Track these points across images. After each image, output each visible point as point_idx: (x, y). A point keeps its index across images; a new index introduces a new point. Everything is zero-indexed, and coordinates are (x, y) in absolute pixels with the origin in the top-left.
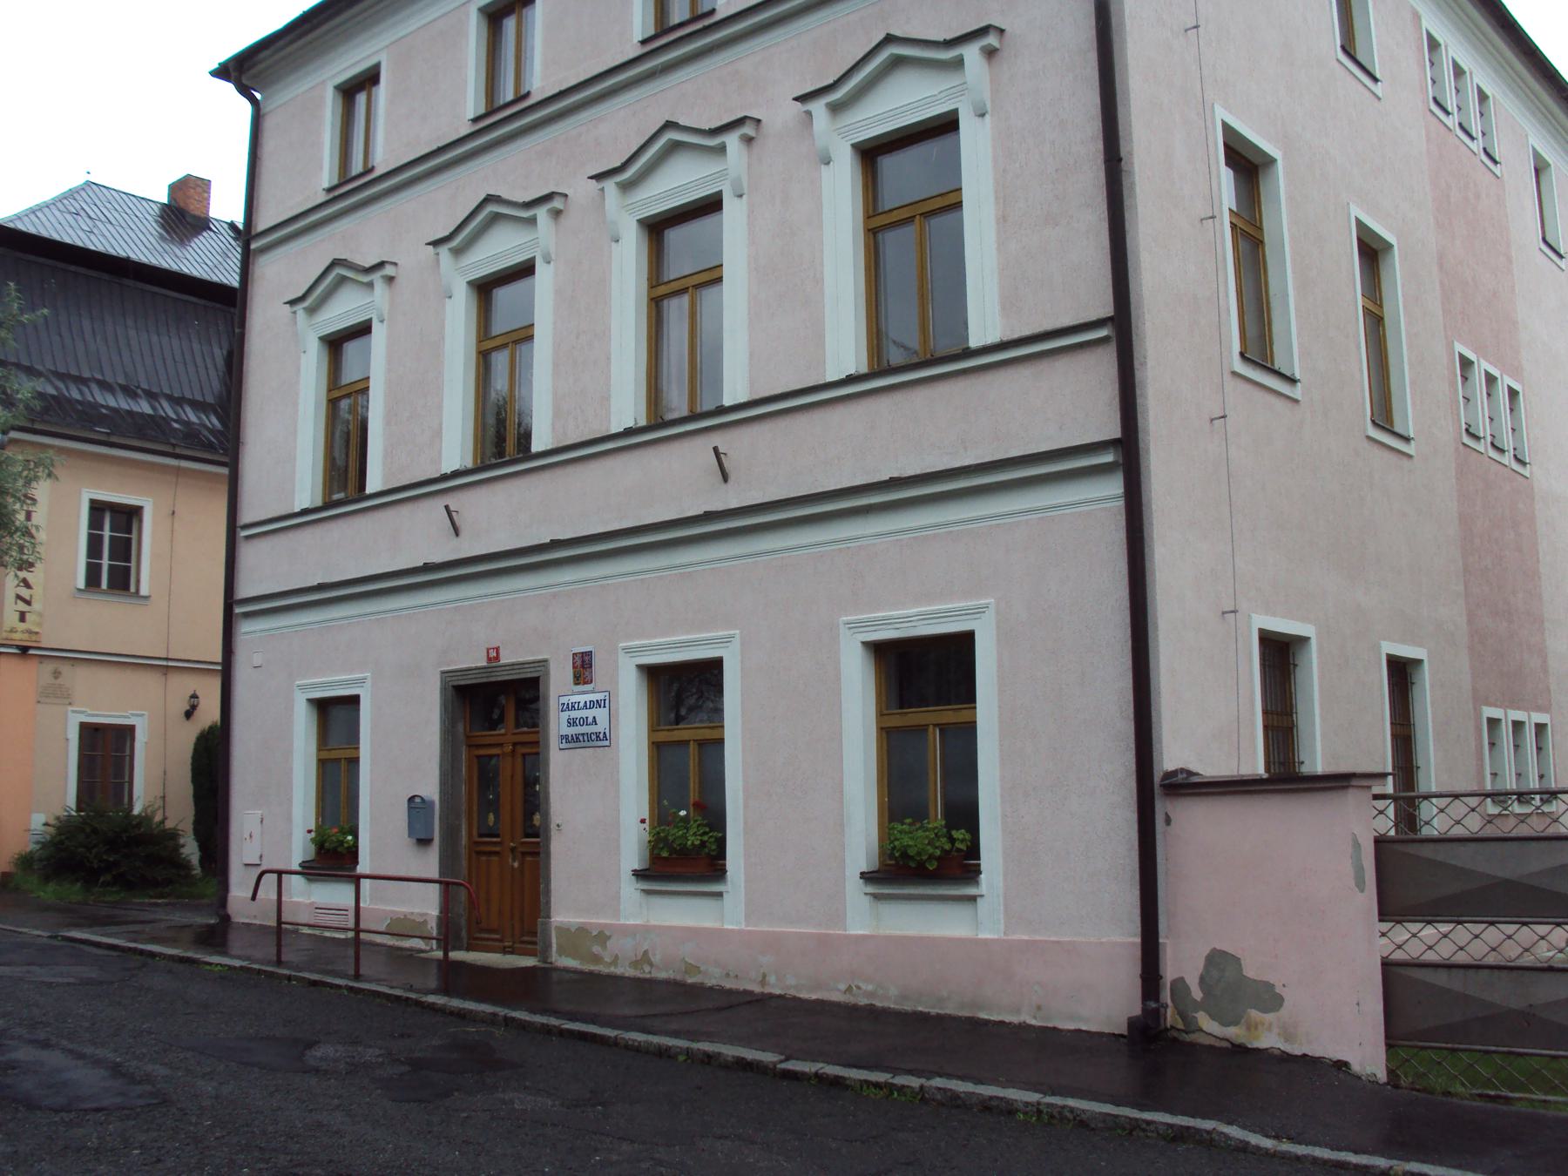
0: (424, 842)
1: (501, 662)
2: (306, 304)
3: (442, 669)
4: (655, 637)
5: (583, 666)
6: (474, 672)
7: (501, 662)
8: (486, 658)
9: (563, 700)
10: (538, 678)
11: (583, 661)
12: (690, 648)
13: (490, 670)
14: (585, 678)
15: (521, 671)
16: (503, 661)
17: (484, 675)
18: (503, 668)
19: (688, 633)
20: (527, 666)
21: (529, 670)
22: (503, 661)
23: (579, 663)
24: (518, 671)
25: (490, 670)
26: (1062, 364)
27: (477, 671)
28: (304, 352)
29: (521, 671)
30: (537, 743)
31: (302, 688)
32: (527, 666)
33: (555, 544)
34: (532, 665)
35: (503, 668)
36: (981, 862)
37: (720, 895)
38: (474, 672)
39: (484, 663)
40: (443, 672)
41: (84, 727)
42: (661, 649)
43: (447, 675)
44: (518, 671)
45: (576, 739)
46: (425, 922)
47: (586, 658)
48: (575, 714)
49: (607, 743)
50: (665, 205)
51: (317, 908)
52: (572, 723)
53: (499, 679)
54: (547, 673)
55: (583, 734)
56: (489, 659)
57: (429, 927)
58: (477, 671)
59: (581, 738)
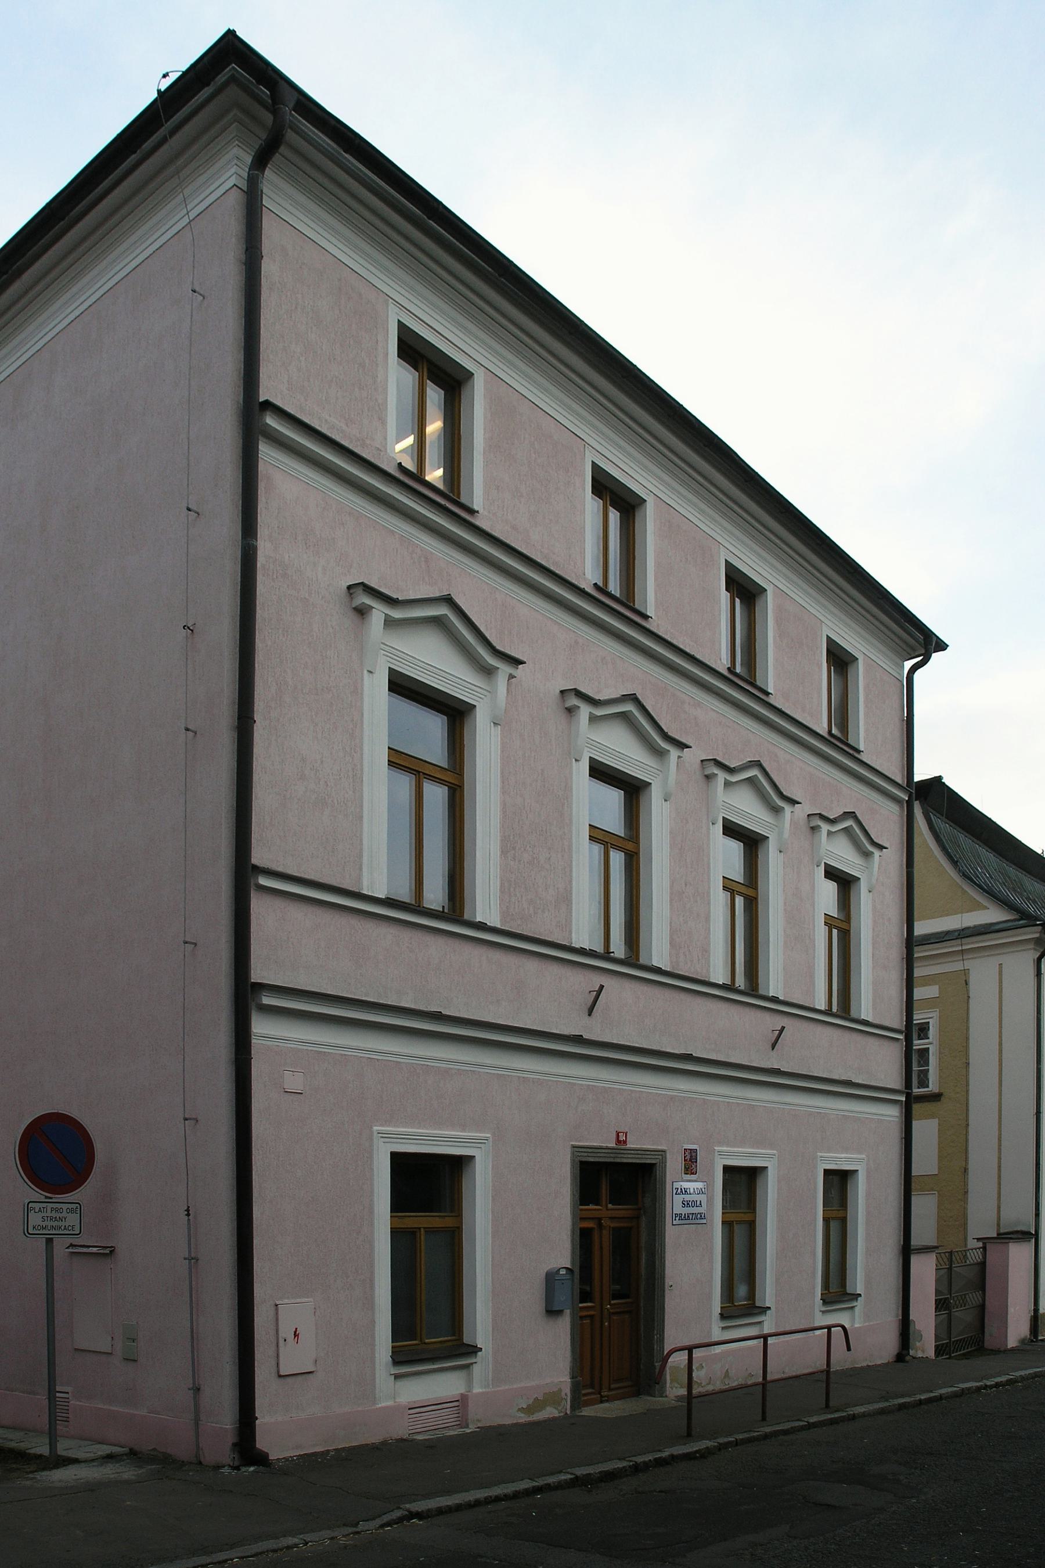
0: (552, 1312)
1: (628, 1146)
2: (397, 614)
3: (573, 1143)
4: (734, 1147)
5: (690, 1160)
6: (604, 1151)
7: (628, 1146)
8: (614, 1140)
9: (676, 1185)
10: (654, 1164)
11: (691, 1156)
12: (754, 1158)
13: (618, 1151)
14: (692, 1170)
15: (644, 1156)
16: (629, 1146)
17: (612, 1155)
18: (629, 1152)
19: (753, 1147)
20: (648, 1153)
21: (649, 1157)
22: (629, 1146)
23: (688, 1157)
24: (640, 1156)
25: (618, 1151)
26: (886, 1043)
27: (606, 1151)
28: (370, 672)
29: (644, 1156)
30: (582, 1219)
31: (386, 1136)
32: (648, 1153)
33: (688, 1058)
34: (652, 1153)
35: (629, 1152)
36: (390, 1344)
37: (467, 1367)
38: (604, 1151)
39: (612, 1144)
40: (574, 1147)
41: (398, 1160)
42: (407, 1139)
43: (577, 1150)
44: (640, 1156)
45: (687, 1217)
46: (560, 1390)
47: (694, 1154)
48: (687, 1197)
49: (704, 1221)
50: (741, 821)
51: (409, 1409)
52: (686, 1204)
53: (625, 1161)
54: (664, 1161)
55: (693, 1214)
56: (618, 1141)
57: (563, 1394)
58: (606, 1151)
59: (691, 1217)
